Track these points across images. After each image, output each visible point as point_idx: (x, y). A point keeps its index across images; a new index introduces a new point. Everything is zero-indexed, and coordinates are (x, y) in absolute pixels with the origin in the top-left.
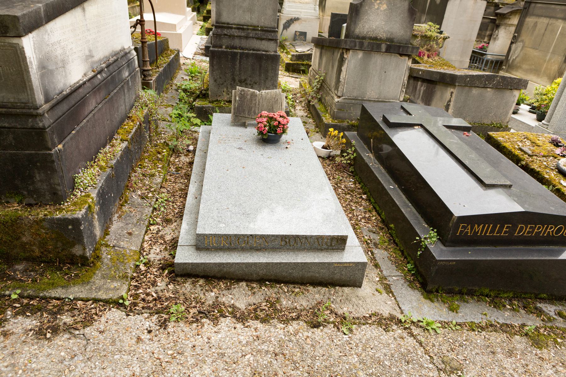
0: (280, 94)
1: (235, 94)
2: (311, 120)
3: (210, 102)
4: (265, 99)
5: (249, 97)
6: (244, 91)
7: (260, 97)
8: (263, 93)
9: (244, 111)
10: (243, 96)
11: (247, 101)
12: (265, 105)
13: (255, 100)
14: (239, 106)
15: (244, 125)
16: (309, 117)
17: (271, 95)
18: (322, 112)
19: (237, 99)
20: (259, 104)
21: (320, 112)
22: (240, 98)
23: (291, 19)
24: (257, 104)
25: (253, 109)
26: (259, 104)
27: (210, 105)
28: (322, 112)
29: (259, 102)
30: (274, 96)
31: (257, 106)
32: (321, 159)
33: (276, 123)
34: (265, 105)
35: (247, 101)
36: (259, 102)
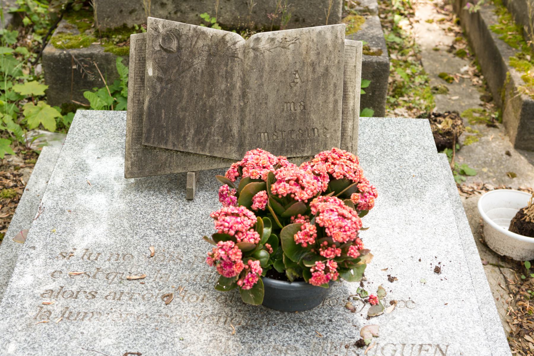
0: (338, 46)
1: (141, 50)
2: (466, 68)
3: (99, 35)
4: (274, 68)
5: (199, 63)
6: (177, 34)
7: (248, 62)
8: (264, 45)
9: (179, 126)
10: (173, 60)
11: (193, 80)
12: (272, 98)
13: (229, 75)
14: (156, 106)
15: (178, 186)
16: (461, 54)
17: (297, 53)
18: (509, 45)
19: (150, 72)
20: (244, 95)
21: (501, 47)
22: (163, 68)
23: (491, 259)
24: (237, 93)
25: (219, 118)
26: (244, 95)
27: (98, 48)
28: (509, 45)
29: (245, 83)
30: (313, 57)
31: (236, 102)
32: (509, 273)
33: (303, 232)
34: (272, 98)
35: (193, 80)
36: (245, 83)
